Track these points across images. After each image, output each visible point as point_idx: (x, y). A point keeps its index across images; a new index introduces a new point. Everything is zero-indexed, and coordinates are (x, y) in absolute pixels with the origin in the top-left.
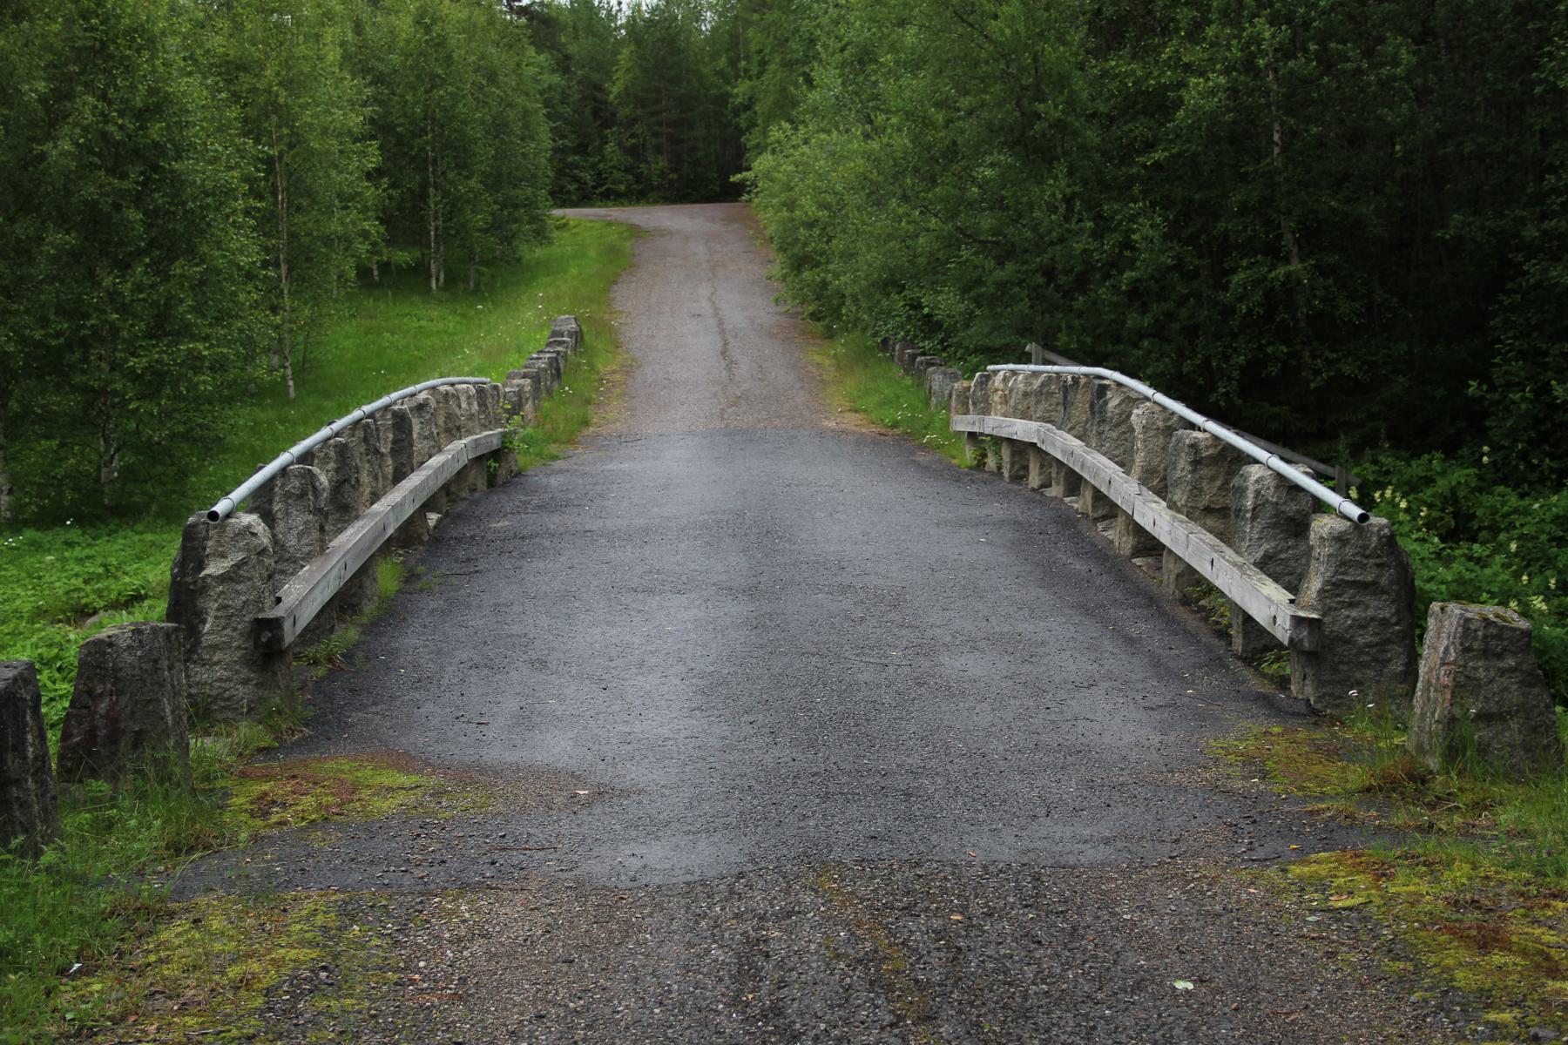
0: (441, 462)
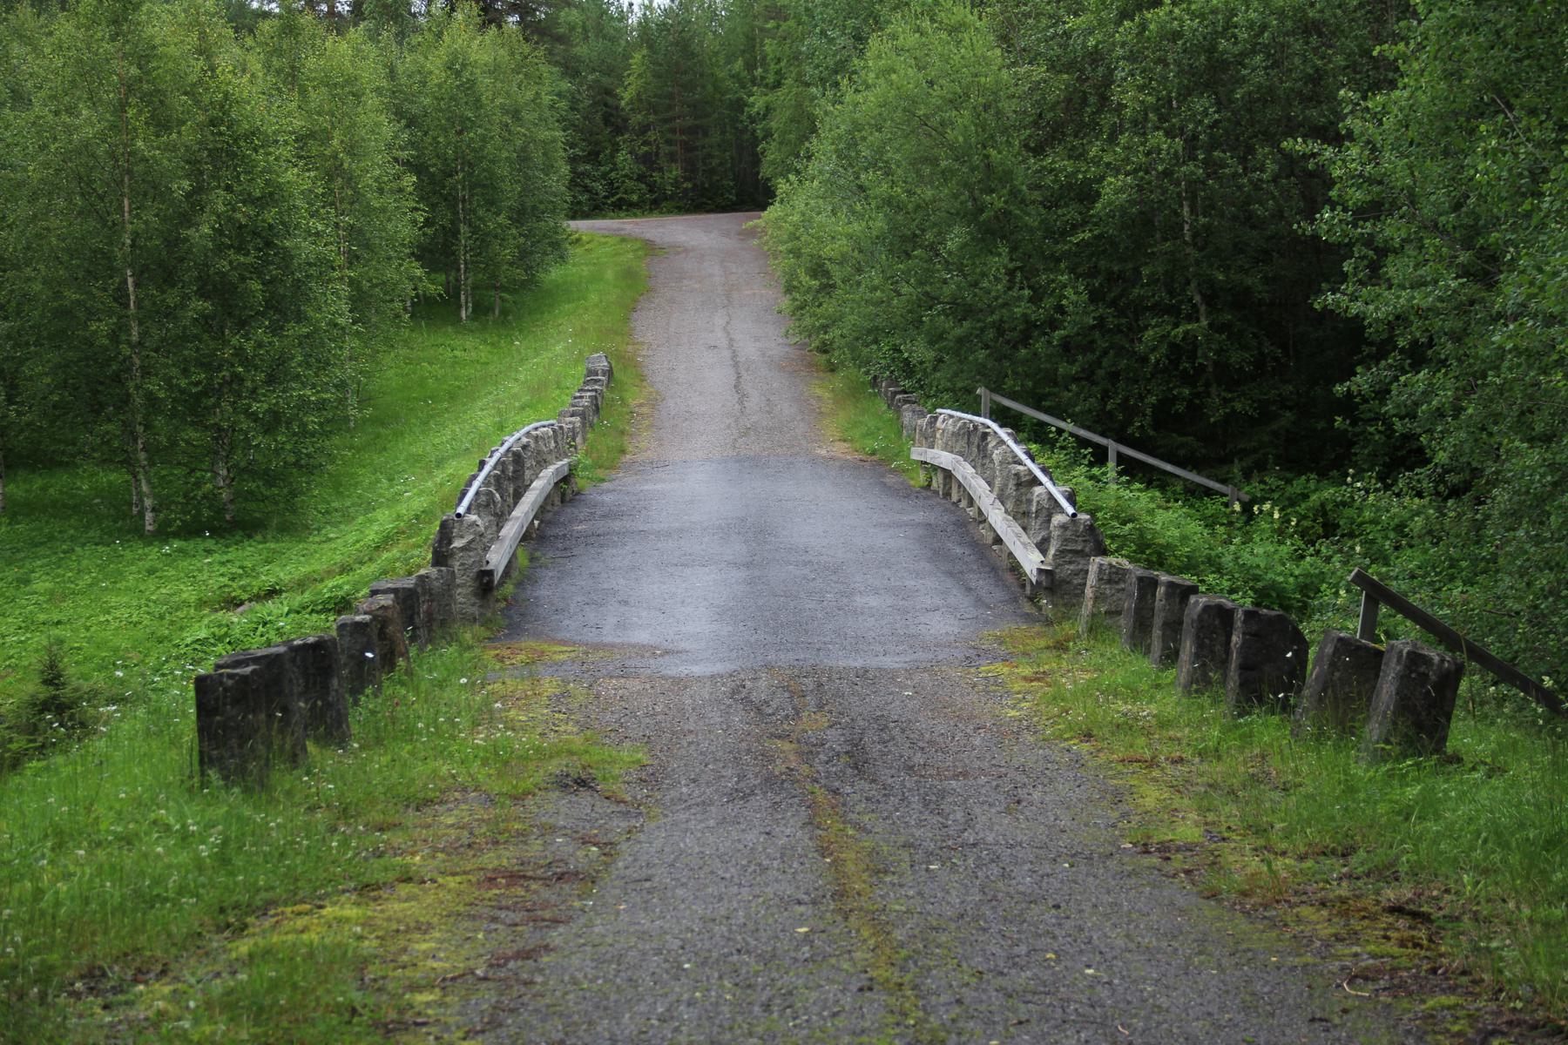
0: (541, 484)
